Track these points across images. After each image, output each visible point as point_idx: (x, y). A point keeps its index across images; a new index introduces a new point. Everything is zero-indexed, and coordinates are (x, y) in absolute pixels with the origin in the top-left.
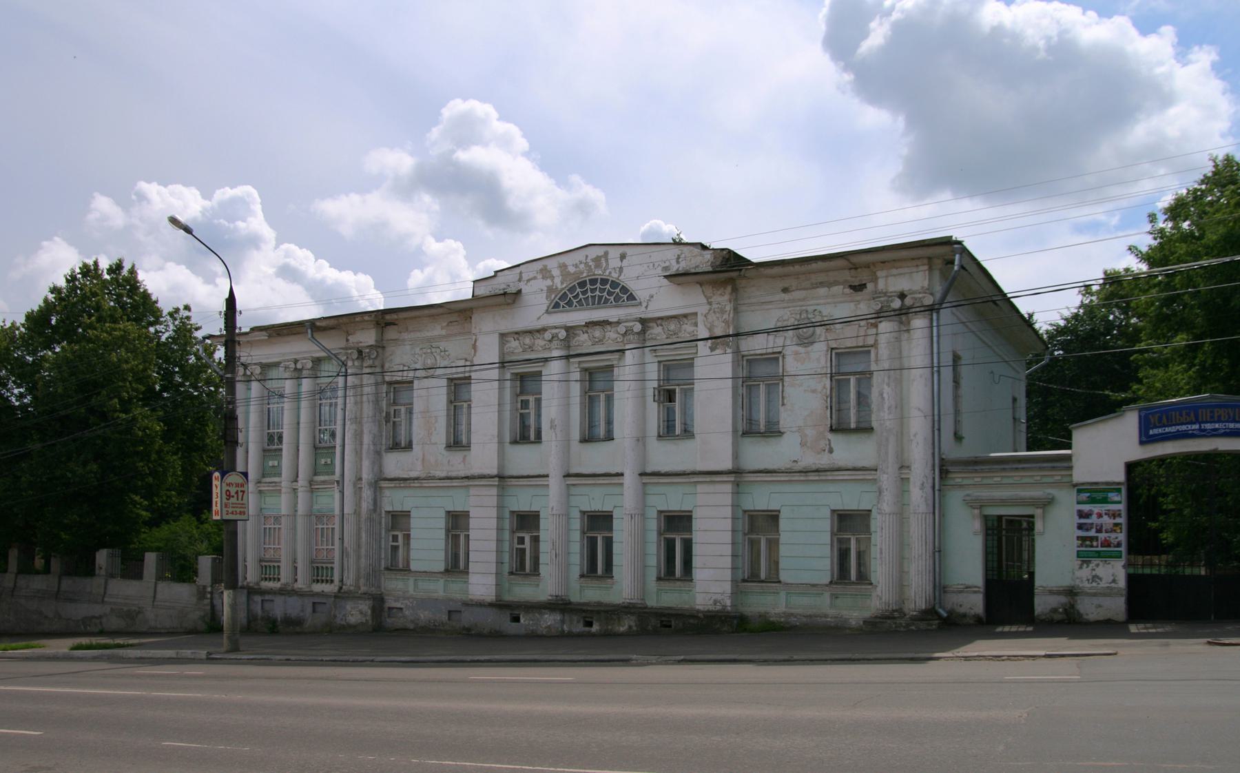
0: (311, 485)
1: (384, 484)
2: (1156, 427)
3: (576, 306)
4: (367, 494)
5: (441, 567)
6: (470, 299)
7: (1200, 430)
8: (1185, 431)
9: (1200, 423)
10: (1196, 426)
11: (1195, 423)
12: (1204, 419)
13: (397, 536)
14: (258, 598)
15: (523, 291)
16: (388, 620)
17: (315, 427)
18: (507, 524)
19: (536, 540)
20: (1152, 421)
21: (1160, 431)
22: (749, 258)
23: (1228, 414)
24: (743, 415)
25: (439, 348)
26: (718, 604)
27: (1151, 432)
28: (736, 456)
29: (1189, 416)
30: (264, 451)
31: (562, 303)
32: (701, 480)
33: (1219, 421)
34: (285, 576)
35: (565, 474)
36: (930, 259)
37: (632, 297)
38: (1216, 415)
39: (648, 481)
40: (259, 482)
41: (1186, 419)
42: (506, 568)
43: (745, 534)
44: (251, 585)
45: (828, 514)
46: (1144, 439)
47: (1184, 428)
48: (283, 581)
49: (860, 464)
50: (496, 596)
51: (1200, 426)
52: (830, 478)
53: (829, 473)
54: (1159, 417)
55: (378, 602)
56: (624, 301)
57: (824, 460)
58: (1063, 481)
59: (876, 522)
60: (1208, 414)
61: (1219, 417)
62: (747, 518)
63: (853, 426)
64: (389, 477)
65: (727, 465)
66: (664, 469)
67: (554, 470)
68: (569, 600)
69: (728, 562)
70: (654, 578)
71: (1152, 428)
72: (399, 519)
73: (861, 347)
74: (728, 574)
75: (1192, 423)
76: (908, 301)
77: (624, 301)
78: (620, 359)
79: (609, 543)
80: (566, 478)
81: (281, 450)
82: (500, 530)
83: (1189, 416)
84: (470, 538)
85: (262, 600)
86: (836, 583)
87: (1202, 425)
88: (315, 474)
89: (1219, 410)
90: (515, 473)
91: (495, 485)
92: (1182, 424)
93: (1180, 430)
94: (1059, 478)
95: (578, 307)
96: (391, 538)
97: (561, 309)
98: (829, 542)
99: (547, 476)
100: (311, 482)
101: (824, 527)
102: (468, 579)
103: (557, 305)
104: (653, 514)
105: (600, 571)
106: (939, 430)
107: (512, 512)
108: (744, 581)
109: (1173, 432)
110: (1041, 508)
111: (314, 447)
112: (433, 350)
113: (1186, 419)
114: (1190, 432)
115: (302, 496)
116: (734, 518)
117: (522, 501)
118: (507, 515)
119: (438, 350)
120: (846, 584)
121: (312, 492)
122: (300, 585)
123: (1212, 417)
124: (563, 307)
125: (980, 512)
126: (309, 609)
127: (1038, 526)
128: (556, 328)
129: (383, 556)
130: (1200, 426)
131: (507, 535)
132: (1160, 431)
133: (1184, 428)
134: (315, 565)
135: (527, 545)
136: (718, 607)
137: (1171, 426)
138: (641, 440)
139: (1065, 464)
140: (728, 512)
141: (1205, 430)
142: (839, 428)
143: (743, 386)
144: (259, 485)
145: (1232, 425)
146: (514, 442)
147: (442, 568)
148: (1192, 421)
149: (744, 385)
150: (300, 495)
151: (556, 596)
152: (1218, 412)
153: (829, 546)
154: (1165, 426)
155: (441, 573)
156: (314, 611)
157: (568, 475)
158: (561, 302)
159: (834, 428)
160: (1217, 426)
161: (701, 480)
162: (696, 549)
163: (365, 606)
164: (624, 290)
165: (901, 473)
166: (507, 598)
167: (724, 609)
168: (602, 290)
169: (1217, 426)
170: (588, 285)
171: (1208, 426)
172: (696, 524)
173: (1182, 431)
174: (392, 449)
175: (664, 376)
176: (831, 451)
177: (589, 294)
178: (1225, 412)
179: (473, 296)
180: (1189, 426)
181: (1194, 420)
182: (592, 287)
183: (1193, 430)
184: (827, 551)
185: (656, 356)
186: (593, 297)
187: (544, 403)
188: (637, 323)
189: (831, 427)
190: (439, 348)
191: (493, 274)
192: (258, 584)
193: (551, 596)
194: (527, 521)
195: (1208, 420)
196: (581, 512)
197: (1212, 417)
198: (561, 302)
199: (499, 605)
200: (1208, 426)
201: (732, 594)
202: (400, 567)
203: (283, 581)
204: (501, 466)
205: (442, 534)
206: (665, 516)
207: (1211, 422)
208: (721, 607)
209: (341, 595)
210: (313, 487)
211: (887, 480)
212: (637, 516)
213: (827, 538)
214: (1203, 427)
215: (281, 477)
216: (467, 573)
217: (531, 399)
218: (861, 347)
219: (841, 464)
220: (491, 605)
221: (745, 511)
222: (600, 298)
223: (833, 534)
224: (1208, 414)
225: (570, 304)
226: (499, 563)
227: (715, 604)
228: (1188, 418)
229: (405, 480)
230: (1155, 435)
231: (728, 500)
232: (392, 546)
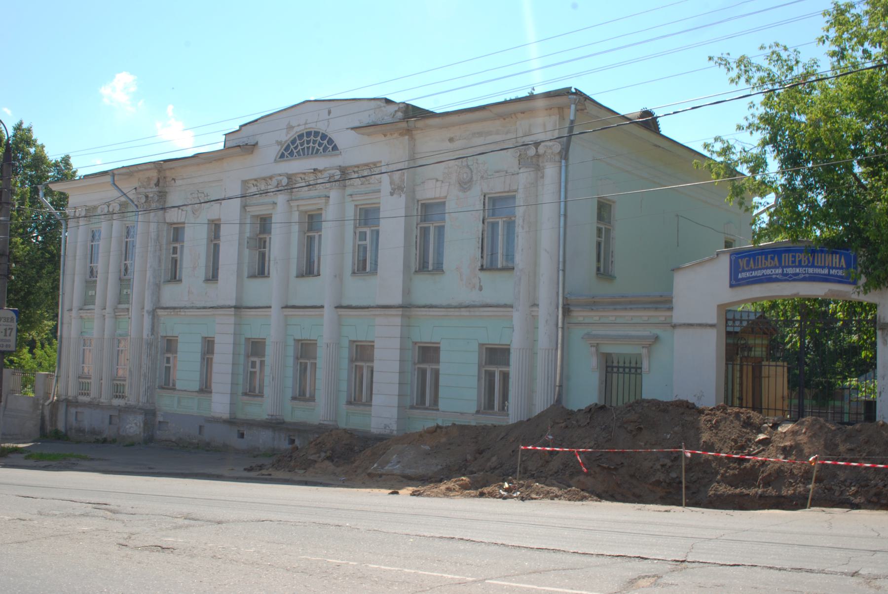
0: (115, 312)
1: (160, 312)
2: (744, 271)
3: (287, 157)
4: (147, 320)
5: (196, 386)
6: (222, 150)
7: (783, 274)
8: (770, 275)
9: (783, 268)
10: (779, 271)
11: (778, 268)
12: (787, 264)
13: (255, 362)
14: (73, 410)
15: (260, 144)
16: (158, 432)
17: (121, 262)
18: (242, 350)
19: (262, 363)
20: (741, 264)
21: (748, 274)
22: (427, 108)
23: (808, 259)
24: (416, 254)
25: (203, 193)
26: (388, 428)
27: (740, 276)
28: (407, 291)
29: (774, 261)
30: (86, 282)
31: (286, 154)
32: (377, 313)
33: (800, 266)
34: (94, 392)
35: (283, 306)
36: (559, 108)
37: (335, 148)
38: (797, 259)
39: (290, 313)
40: (81, 309)
41: (771, 263)
42: (240, 390)
43: (415, 364)
44: (70, 398)
45: (476, 348)
46: (734, 283)
47: (768, 272)
48: (92, 396)
49: (502, 302)
50: (230, 414)
51: (783, 271)
52: (477, 314)
53: (476, 309)
54: (747, 260)
55: (150, 414)
56: (329, 151)
57: (473, 297)
58: (616, 322)
59: (514, 357)
60: (790, 259)
61: (800, 261)
62: (484, 351)
63: (500, 266)
64: (164, 306)
65: (398, 300)
66: (354, 304)
67: (328, 302)
68: (283, 420)
69: (395, 389)
70: (344, 402)
71: (741, 272)
72: (170, 345)
73: (508, 192)
74: (395, 401)
75: (775, 267)
76: (541, 150)
77: (329, 151)
78: (274, 208)
79: (505, 377)
80: (284, 310)
81: (96, 281)
82: (235, 354)
83: (774, 261)
84: (317, 366)
85: (76, 412)
86: (483, 413)
87: (785, 270)
88: (120, 303)
89: (800, 254)
90: (249, 305)
91: (232, 315)
92: (767, 268)
93: (765, 274)
94: (613, 318)
95: (297, 157)
96: (250, 364)
97: (285, 158)
98: (476, 374)
99: (270, 307)
100: (115, 309)
101: (473, 358)
102: (211, 397)
103: (282, 156)
104: (345, 343)
105: (427, 404)
106: (564, 270)
107: (247, 339)
108: (412, 407)
109: (759, 276)
110: (646, 347)
111: (120, 279)
112: (200, 195)
113: (771, 263)
114: (774, 276)
115: (108, 322)
116: (402, 349)
117: (254, 331)
118: (243, 341)
119: (203, 195)
120: (491, 414)
121: (116, 318)
122: (104, 400)
123: (794, 262)
124: (287, 157)
125: (597, 350)
126: (107, 421)
127: (645, 365)
128: (280, 175)
129: (158, 376)
130: (783, 271)
131: (242, 359)
132: (748, 274)
133: (768, 272)
134: (115, 382)
135: (365, 372)
136: (387, 431)
137: (757, 270)
138: (339, 276)
139: (667, 306)
140: (397, 343)
141: (787, 275)
142: (488, 267)
143: (417, 228)
144: (81, 311)
145: (811, 270)
146: (252, 276)
147: (197, 389)
148: (775, 265)
149: (419, 228)
150: (107, 320)
151: (272, 416)
152: (799, 257)
153: (476, 378)
154: (752, 270)
155: (197, 392)
156: (110, 423)
157: (286, 307)
158: (288, 151)
159: (485, 267)
160: (798, 270)
161: (377, 313)
162: (442, 381)
163: (140, 418)
164: (331, 141)
165: (532, 311)
166: (240, 416)
167: (392, 433)
168: (315, 142)
169: (798, 270)
170: (312, 137)
171: (790, 271)
172: (443, 356)
173: (767, 275)
174: (169, 281)
175: (421, 212)
176: (481, 289)
177: (306, 145)
178: (805, 257)
179: (224, 147)
180: (773, 270)
181: (777, 265)
182: (308, 139)
183: (777, 274)
184: (474, 382)
185: (353, 200)
186: (303, 149)
187: (323, 238)
188: (338, 171)
189: (482, 266)
190: (203, 193)
191: (238, 128)
192: (76, 397)
193: (268, 415)
194: (256, 347)
195: (790, 264)
196: (294, 340)
197: (794, 262)
198: (288, 151)
199: (231, 422)
200: (790, 271)
201: (398, 419)
202: (168, 385)
203: (92, 396)
204: (239, 297)
205: (198, 357)
206: (419, 347)
207: (792, 267)
208: (389, 431)
209: (128, 409)
210: (117, 314)
211: (518, 317)
212: (332, 345)
213: (474, 370)
214: (785, 272)
215: (95, 304)
216: (262, 396)
217: (317, 235)
218: (508, 192)
219: (489, 301)
220: (226, 422)
221: (416, 343)
222: (313, 148)
223: (480, 366)
224: (790, 259)
225: (291, 154)
226: (234, 384)
227: (385, 428)
228: (772, 262)
229: (174, 308)
230: (743, 279)
231: (397, 332)
232: (166, 367)
